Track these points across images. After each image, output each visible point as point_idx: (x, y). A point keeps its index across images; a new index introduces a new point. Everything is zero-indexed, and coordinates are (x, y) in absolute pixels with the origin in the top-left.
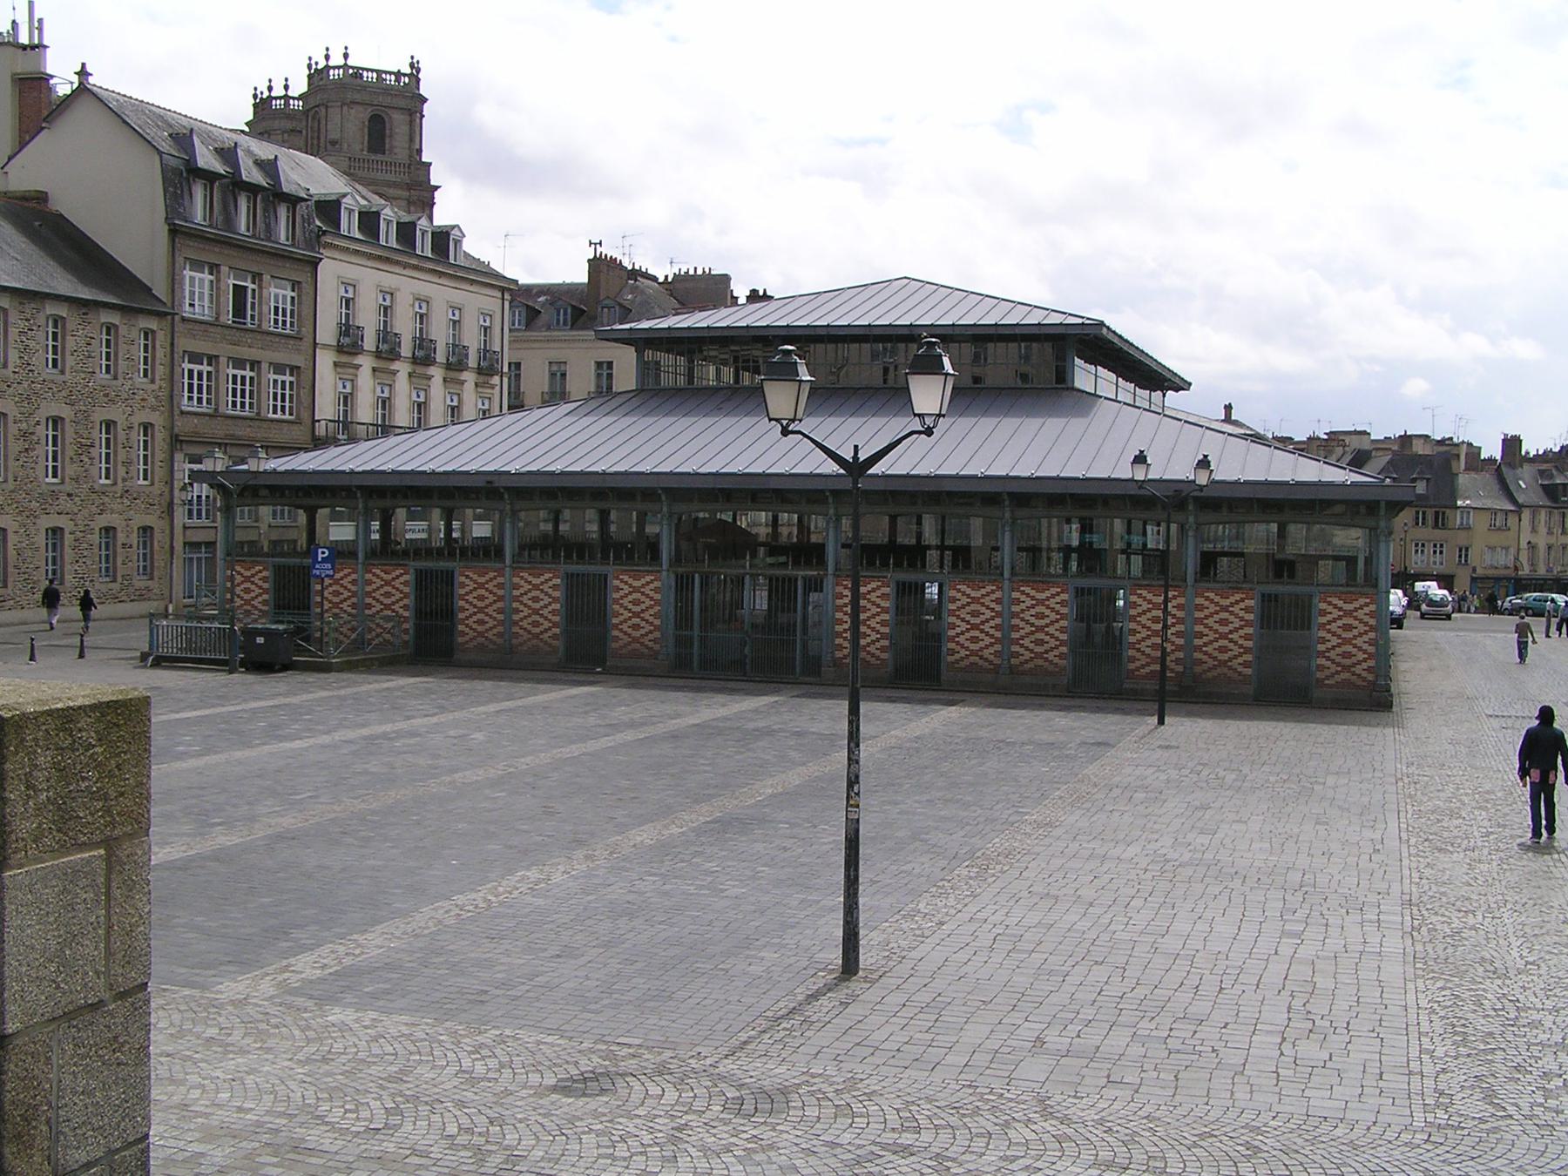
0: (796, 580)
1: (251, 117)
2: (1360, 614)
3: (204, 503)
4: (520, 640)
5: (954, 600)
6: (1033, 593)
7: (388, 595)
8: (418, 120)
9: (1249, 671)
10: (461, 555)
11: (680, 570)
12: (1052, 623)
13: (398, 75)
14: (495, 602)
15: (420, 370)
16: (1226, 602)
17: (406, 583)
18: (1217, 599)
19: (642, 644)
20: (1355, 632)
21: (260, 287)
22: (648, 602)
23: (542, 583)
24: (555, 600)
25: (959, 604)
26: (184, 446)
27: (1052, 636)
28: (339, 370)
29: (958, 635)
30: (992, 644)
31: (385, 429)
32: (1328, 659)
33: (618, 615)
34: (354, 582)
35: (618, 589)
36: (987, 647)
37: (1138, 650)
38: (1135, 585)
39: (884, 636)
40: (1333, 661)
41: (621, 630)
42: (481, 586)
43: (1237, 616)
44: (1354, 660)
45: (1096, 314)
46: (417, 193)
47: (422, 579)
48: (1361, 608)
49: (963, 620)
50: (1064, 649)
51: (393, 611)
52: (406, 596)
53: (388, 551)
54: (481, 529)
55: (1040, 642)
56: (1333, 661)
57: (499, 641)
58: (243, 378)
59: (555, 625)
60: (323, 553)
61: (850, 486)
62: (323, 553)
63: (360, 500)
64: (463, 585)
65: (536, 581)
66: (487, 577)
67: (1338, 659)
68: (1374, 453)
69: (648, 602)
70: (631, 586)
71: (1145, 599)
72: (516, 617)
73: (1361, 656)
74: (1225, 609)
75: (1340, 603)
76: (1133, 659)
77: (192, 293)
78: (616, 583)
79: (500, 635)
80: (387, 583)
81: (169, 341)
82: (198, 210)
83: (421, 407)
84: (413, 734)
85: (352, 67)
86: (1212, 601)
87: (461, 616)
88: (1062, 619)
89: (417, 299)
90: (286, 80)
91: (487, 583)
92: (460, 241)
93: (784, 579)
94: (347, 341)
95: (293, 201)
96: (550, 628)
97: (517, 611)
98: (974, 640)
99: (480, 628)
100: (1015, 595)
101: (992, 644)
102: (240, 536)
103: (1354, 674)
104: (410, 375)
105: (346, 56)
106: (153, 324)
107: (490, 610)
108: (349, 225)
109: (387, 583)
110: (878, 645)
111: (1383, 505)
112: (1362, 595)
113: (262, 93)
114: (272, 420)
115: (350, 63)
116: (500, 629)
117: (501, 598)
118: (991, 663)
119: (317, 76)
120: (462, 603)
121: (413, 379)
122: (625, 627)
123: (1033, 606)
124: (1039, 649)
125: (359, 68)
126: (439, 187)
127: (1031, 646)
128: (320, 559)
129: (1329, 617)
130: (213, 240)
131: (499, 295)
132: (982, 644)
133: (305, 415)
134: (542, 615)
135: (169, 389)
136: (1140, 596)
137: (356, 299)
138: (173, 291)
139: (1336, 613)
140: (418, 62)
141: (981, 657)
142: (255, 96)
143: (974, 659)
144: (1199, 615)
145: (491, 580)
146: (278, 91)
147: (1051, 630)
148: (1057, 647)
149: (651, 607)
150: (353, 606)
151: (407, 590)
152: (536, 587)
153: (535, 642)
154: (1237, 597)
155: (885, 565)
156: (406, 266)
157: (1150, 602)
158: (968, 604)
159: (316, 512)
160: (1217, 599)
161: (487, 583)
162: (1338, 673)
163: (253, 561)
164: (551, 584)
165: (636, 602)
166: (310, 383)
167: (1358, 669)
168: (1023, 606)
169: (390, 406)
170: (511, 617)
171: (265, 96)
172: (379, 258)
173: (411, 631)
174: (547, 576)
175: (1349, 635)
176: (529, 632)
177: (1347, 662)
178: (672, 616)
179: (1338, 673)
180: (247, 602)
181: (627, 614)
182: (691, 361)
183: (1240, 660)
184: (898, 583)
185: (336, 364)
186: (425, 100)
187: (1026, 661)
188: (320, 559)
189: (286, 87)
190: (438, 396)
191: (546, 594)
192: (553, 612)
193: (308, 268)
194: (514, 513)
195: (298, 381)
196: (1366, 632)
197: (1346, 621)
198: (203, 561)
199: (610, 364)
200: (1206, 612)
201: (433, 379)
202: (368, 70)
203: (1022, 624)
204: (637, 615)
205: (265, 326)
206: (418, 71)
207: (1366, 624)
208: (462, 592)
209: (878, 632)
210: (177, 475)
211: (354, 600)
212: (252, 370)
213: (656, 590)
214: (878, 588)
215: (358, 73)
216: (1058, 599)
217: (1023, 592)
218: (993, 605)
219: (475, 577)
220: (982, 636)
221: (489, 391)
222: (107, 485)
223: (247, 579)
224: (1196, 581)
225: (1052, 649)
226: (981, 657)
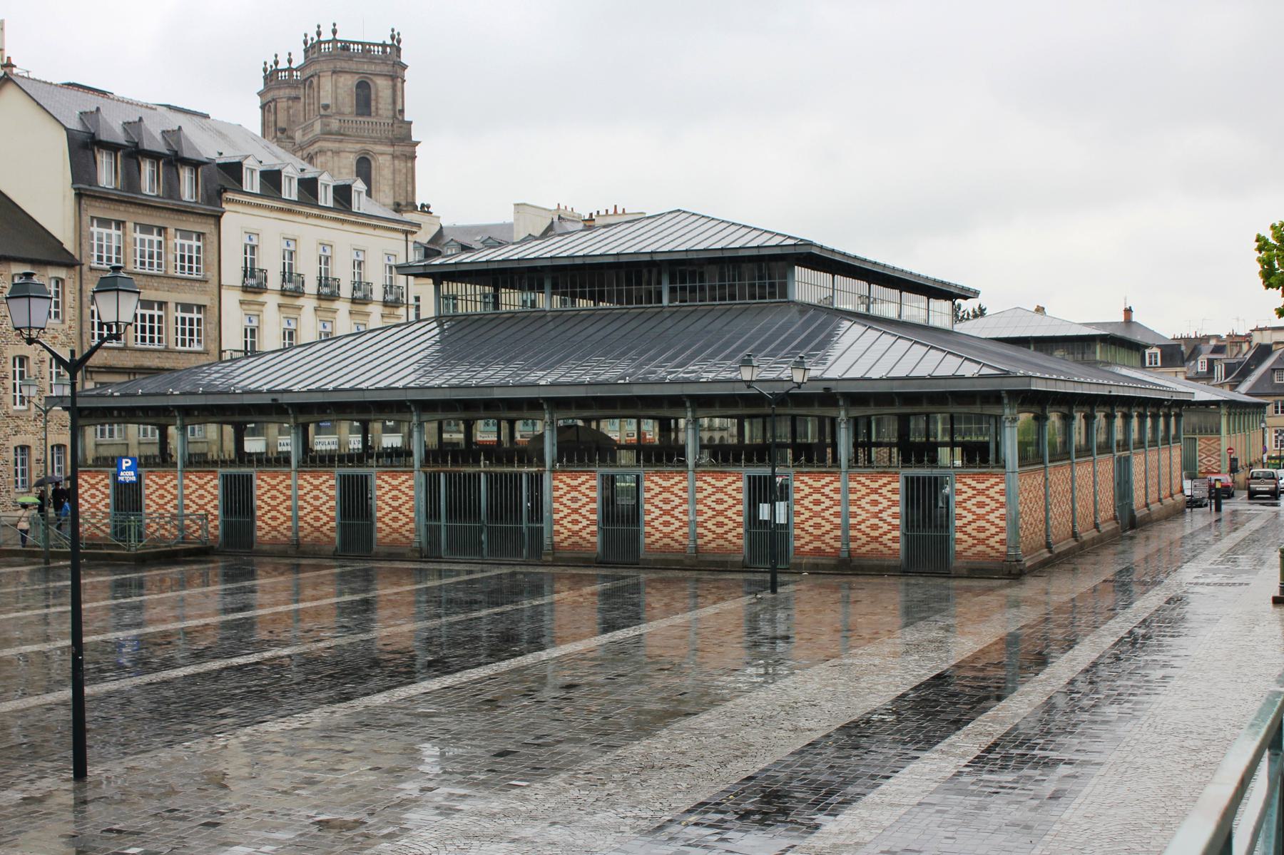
0: (521, 476)
1: (262, 87)
2: (992, 492)
4: (306, 532)
5: (649, 490)
6: (713, 482)
7: (201, 497)
9: (896, 546)
10: (339, 461)
11: (429, 469)
12: (730, 507)
13: (384, 45)
14: (285, 501)
15: (325, 304)
17: (215, 487)
18: (868, 482)
19: (401, 534)
20: (988, 509)
21: (166, 239)
22: (404, 498)
23: (321, 484)
24: (332, 498)
25: (653, 493)
26: (94, 376)
27: (730, 519)
28: (244, 307)
29: (653, 520)
30: (681, 528)
31: (251, 351)
32: (965, 533)
33: (380, 509)
34: (175, 487)
35: (380, 487)
36: (677, 529)
37: (803, 529)
38: (798, 472)
39: (593, 522)
40: (970, 535)
41: (384, 523)
42: (274, 487)
43: (885, 497)
44: (988, 533)
46: (400, 148)
47: (228, 482)
48: (992, 486)
49: (657, 507)
50: (741, 530)
53: (313, 460)
54: (392, 441)
55: (720, 525)
56: (970, 535)
57: (289, 534)
58: (152, 317)
59: (332, 519)
64: (259, 487)
65: (316, 482)
66: (278, 480)
68: (1274, 348)
69: (404, 498)
72: (301, 513)
73: (993, 530)
74: (875, 491)
75: (974, 483)
76: (798, 537)
78: (379, 482)
79: (289, 529)
80: (201, 487)
81: (78, 287)
82: (106, 174)
85: (341, 41)
86: (863, 485)
87: (259, 513)
90: (290, 54)
95: (195, 165)
96: (328, 522)
97: (302, 508)
98: (666, 524)
99: (274, 524)
100: (699, 484)
101: (681, 528)
102: (194, 449)
103: (988, 546)
105: (334, 32)
106: (62, 273)
107: (583, 511)
108: (252, 183)
109: (201, 487)
110: (588, 530)
112: (992, 475)
114: (180, 352)
115: (338, 37)
116: (290, 524)
117: (289, 498)
118: (681, 543)
119: (312, 49)
120: (259, 503)
121: (319, 313)
122: (386, 520)
123: (713, 494)
124: (719, 531)
125: (346, 42)
127: (714, 528)
129: (965, 496)
130: (116, 200)
132: (673, 527)
133: (213, 347)
134: (321, 511)
135: (78, 328)
136: (802, 482)
138: (80, 244)
139: (970, 492)
140: (399, 34)
141: (673, 539)
142: (265, 70)
143: (666, 540)
144: (853, 497)
146: (283, 64)
147: (729, 513)
148: (734, 529)
149: (407, 502)
150: (175, 507)
151: (216, 492)
152: (316, 488)
153: (316, 534)
154: (885, 480)
155: (591, 460)
156: (308, 215)
157: (811, 487)
158: (660, 493)
160: (868, 482)
162: (974, 545)
163: (96, 471)
164: (327, 484)
165: (395, 498)
166: (216, 320)
167: (992, 542)
168: (705, 493)
170: (297, 513)
172: (281, 210)
173: (220, 527)
174: (325, 478)
176: (312, 526)
177: (982, 536)
178: (423, 509)
179: (974, 545)
180: (94, 506)
181: (388, 509)
182: (496, 290)
183: (890, 536)
184: (907, 478)
186: (404, 67)
187: (710, 542)
190: (343, 322)
191: (404, 493)
192: (331, 508)
193: (212, 221)
194: (420, 424)
196: (997, 509)
197: (980, 498)
200: (859, 494)
202: (354, 43)
203: (705, 509)
205: (171, 272)
206: (399, 42)
207: (997, 501)
208: (148, 492)
211: (176, 502)
212: (199, 312)
213: (410, 487)
214: (587, 481)
215: (346, 46)
216: (734, 486)
217: (705, 482)
218: (680, 493)
219: (268, 480)
220: (673, 520)
222: (21, 411)
223: (93, 486)
224: (849, 467)
226: (673, 539)
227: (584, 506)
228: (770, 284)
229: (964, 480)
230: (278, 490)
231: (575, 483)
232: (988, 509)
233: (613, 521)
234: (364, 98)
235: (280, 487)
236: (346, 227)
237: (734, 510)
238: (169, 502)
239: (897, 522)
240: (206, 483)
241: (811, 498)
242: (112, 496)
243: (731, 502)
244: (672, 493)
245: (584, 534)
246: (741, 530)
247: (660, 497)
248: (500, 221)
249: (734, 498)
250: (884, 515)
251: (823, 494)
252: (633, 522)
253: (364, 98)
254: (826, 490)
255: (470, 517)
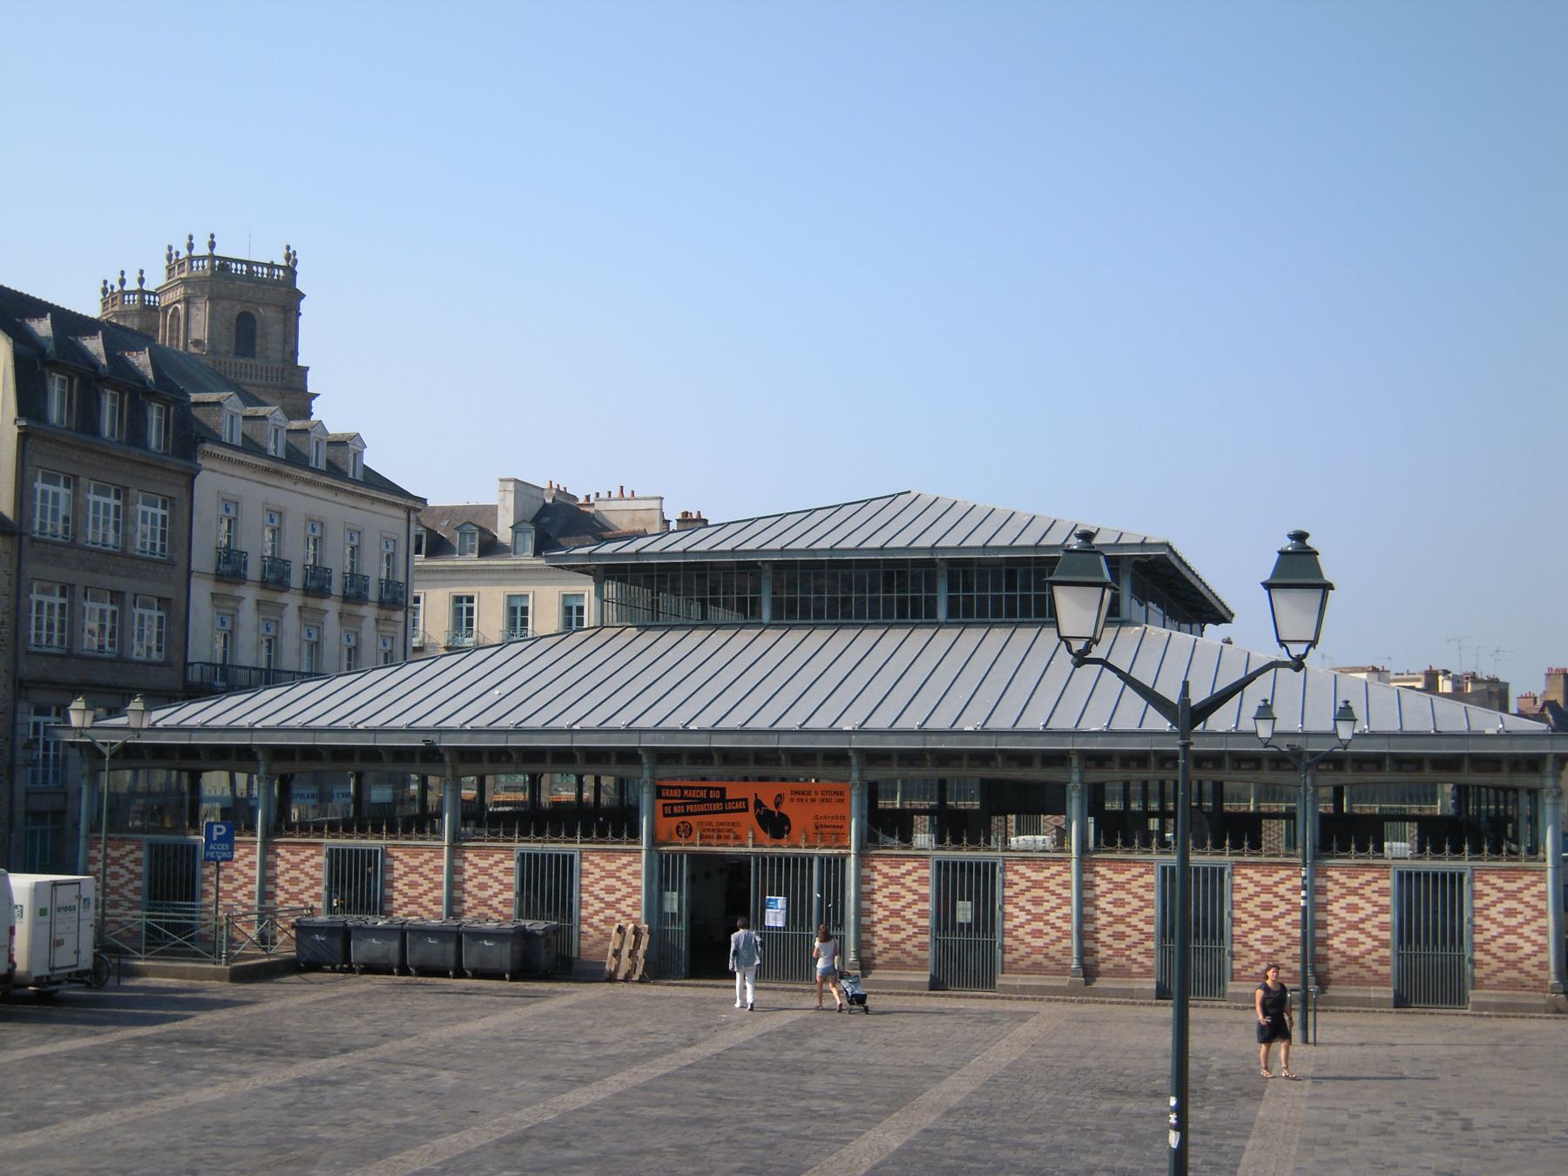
0: (811, 861)
3: (51, 763)
8: (293, 320)
12: (1135, 912)
13: (272, 266)
15: (312, 602)
16: (1354, 883)
17: (317, 867)
20: (1520, 918)
21: (126, 503)
23: (491, 866)
27: (1135, 928)
39: (923, 930)
43: (1368, 900)
45: (1155, 535)
48: (1527, 887)
51: (301, 901)
52: (924, 898)
56: (1494, 956)
60: (219, 830)
61: (1174, 745)
62: (219, 830)
63: (262, 763)
67: (1501, 953)
70: (603, 869)
71: (1251, 880)
77: (44, 510)
83: (315, 647)
84: (360, 1075)
85: (219, 258)
88: (1147, 906)
89: (309, 520)
91: (421, 867)
92: (361, 453)
93: (780, 860)
94: (228, 568)
103: (1521, 971)
104: (300, 609)
105: (212, 245)
110: (915, 941)
111: (1550, 760)
112: (1526, 870)
113: (112, 287)
115: (217, 252)
119: (173, 263)
126: (318, 395)
128: (215, 838)
131: (404, 515)
137: (239, 517)
139: (1495, 895)
140: (295, 253)
142: (105, 291)
145: (427, 862)
146: (132, 284)
147: (1134, 920)
148: (1141, 942)
156: (298, 480)
157: (1257, 884)
158: (1028, 889)
159: (201, 777)
161: (421, 865)
162: (1501, 970)
164: (502, 867)
167: (1527, 965)
169: (276, 646)
171: (115, 291)
172: (267, 470)
175: (1512, 922)
177: (1512, 956)
179: (1501, 970)
183: (1375, 956)
185: (214, 596)
186: (302, 296)
188: (215, 838)
189: (141, 281)
195: (167, 617)
198: (39, 835)
199: (470, 599)
201: (327, 615)
202: (237, 261)
204: (610, 905)
206: (295, 262)
209: (915, 925)
210: (20, 730)
215: (225, 262)
216: (1141, 881)
221: (391, 629)
225: (1135, 945)
227: (909, 905)
228: (871, 599)
229: (1016, 868)
230: (421, 874)
231: (896, 872)
232: (1520, 918)
233: (362, 907)
234: (245, 333)
235: (425, 870)
236: (341, 498)
237: (1141, 915)
238: (240, 888)
239: (1387, 935)
240: (303, 861)
241: (1257, 900)
242: (146, 877)
243: (1136, 903)
244: (1047, 890)
245: (908, 947)
246: (1151, 945)
247: (1028, 895)
248: (463, 503)
249: (1141, 899)
250: (1367, 926)
251: (1276, 895)
252: (985, 929)
253: (245, 333)
254: (1281, 890)
255: (549, 910)
